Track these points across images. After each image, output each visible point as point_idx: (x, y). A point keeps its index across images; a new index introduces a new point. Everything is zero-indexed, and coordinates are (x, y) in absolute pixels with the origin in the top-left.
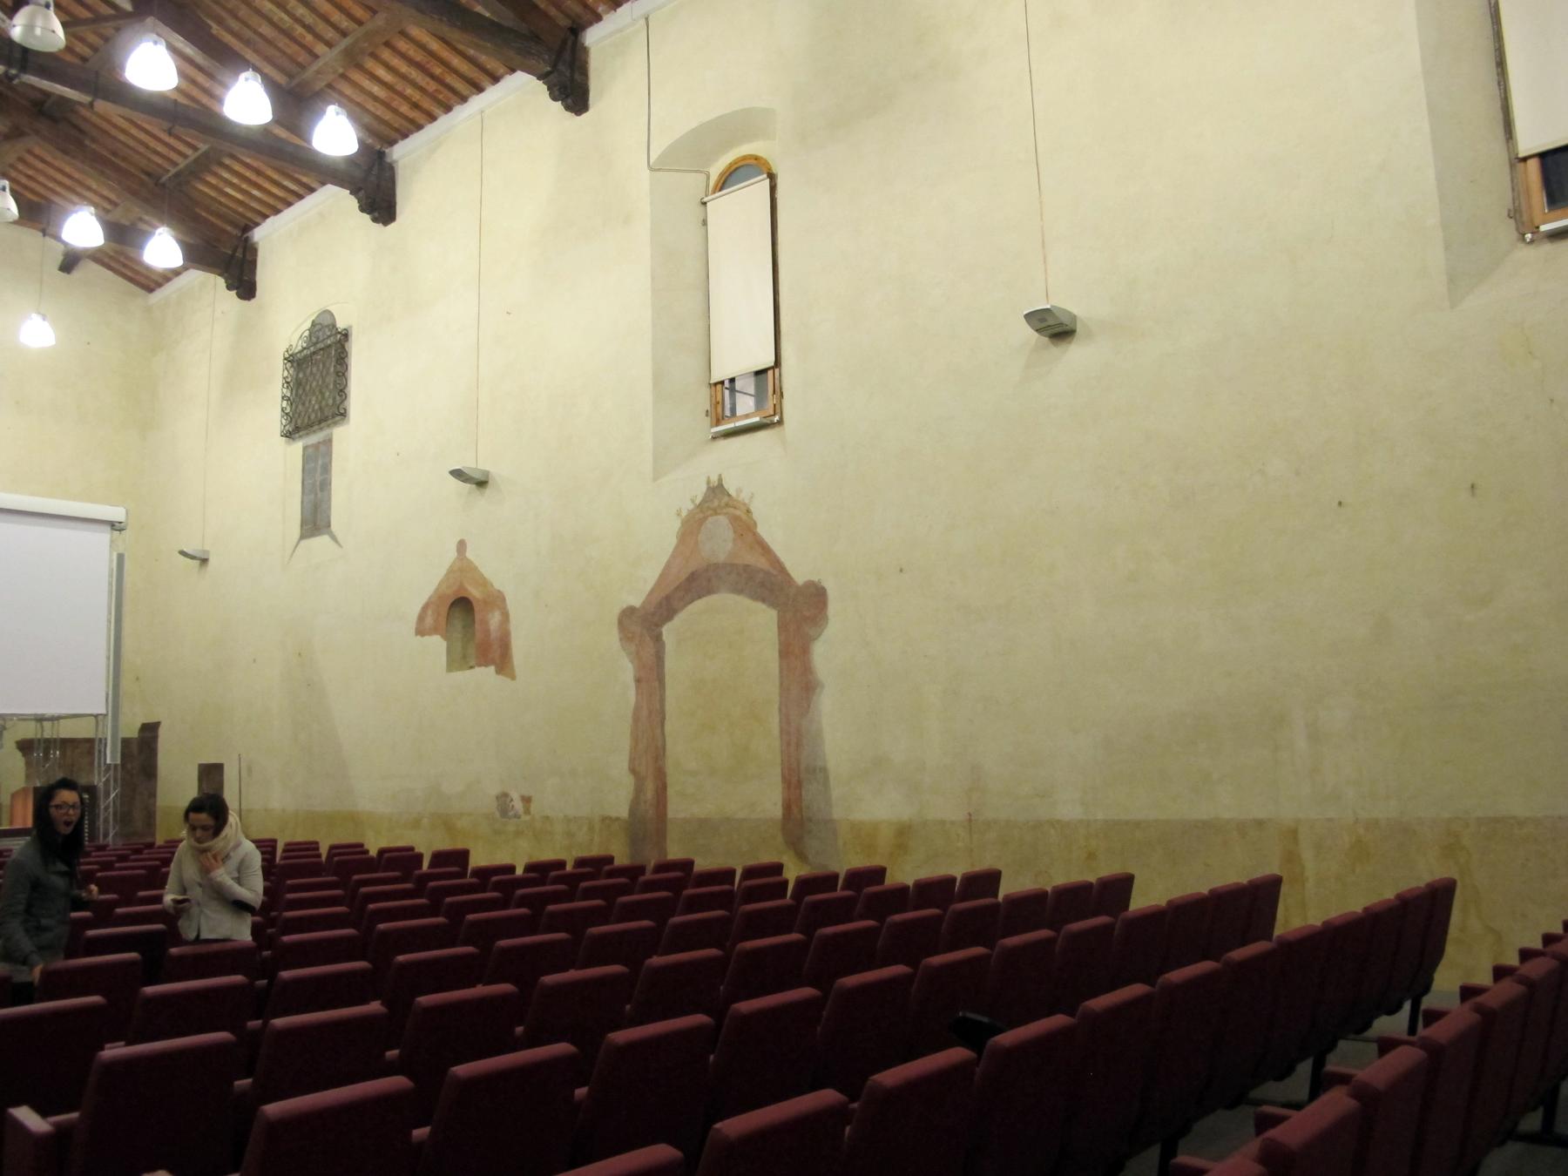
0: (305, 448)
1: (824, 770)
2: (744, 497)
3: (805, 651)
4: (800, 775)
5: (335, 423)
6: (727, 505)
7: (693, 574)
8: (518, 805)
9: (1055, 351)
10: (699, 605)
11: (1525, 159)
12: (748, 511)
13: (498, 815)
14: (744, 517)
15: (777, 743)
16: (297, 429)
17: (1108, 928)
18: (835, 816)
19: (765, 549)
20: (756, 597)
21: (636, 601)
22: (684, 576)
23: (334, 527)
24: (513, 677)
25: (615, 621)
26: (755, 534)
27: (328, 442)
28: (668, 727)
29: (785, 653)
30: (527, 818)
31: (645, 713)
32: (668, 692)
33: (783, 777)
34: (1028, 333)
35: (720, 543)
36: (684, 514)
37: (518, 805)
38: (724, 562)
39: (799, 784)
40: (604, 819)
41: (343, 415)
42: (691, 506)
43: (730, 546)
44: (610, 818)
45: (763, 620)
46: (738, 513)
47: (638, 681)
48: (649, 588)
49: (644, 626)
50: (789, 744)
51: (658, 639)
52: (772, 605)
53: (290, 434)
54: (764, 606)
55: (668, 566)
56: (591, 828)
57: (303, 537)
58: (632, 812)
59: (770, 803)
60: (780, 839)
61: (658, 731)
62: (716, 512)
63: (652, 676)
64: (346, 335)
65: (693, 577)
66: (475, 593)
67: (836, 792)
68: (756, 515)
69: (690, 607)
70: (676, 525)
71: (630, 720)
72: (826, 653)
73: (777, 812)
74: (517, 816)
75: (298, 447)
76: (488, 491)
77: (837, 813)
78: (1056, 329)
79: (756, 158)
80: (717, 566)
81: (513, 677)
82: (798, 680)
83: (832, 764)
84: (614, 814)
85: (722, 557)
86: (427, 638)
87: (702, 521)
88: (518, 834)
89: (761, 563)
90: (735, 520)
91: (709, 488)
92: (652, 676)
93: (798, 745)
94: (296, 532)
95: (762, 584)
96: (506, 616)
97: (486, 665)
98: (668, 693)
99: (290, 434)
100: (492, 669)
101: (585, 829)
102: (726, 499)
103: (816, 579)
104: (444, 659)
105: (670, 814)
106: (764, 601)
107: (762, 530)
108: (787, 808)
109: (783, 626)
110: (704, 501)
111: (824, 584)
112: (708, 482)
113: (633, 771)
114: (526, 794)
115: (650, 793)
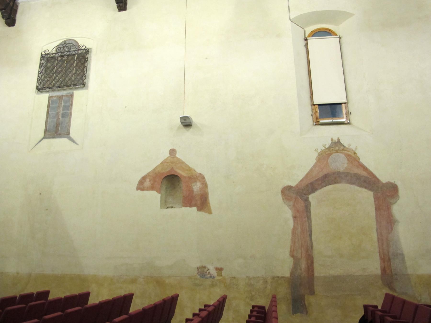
0: (50, 97)
1: (402, 255)
2: (353, 147)
3: (389, 208)
4: (389, 257)
5: (77, 89)
6: (343, 150)
7: (326, 175)
8: (213, 272)
9: (184, 130)
10: (330, 187)
11: (314, 105)
12: (355, 153)
13: (198, 277)
14: (353, 155)
15: (377, 245)
16: (44, 88)
17: (43, 304)
18: (409, 273)
19: (365, 169)
20: (361, 186)
21: (293, 184)
22: (321, 175)
23: (72, 134)
24: (210, 213)
25: (280, 191)
26: (359, 162)
27: (72, 96)
28: (313, 237)
29: (378, 208)
30: (220, 278)
31: (299, 230)
32: (313, 222)
33: (381, 258)
34: (179, 122)
35: (340, 163)
36: (319, 151)
37: (213, 272)
38: (338, 171)
39: (389, 260)
40: (273, 278)
41: (83, 85)
42: (323, 148)
43: (346, 165)
44: (278, 277)
45: (366, 196)
46: (349, 153)
47: (295, 217)
48: (300, 178)
49: (299, 195)
50: (382, 245)
51: (307, 200)
52: (371, 190)
53: (40, 89)
54: (366, 190)
55: (311, 170)
56: (265, 281)
57: (45, 138)
58: (292, 274)
59: (374, 267)
60: (380, 282)
61: (308, 238)
62: (337, 152)
63: (303, 214)
64: (87, 51)
65: (326, 176)
66: (180, 172)
67: (408, 263)
68: (358, 155)
69: (325, 188)
70: (316, 155)
71: (290, 234)
72: (397, 209)
73: (379, 272)
74: (212, 277)
75: (45, 97)
76: (191, 130)
77: (410, 271)
78: (187, 123)
79: (330, 30)
80: (339, 173)
81: (210, 213)
82: (386, 220)
83: (405, 252)
84: (280, 275)
85: (342, 170)
86: (145, 192)
87: (330, 155)
88: (213, 285)
89: (364, 173)
90: (348, 156)
91: (332, 142)
92: (303, 214)
93: (388, 245)
94: (42, 135)
95: (365, 181)
96: (205, 185)
97: (191, 206)
98: (313, 222)
99: (40, 89)
100: (195, 208)
101: (261, 282)
102: (342, 147)
103: (393, 181)
104: (159, 203)
105: (316, 274)
106: (366, 188)
107: (362, 161)
108: (384, 270)
109: (376, 198)
110: (330, 147)
111: (396, 183)
112: (332, 140)
113: (292, 256)
114: (219, 266)
115: (303, 264)
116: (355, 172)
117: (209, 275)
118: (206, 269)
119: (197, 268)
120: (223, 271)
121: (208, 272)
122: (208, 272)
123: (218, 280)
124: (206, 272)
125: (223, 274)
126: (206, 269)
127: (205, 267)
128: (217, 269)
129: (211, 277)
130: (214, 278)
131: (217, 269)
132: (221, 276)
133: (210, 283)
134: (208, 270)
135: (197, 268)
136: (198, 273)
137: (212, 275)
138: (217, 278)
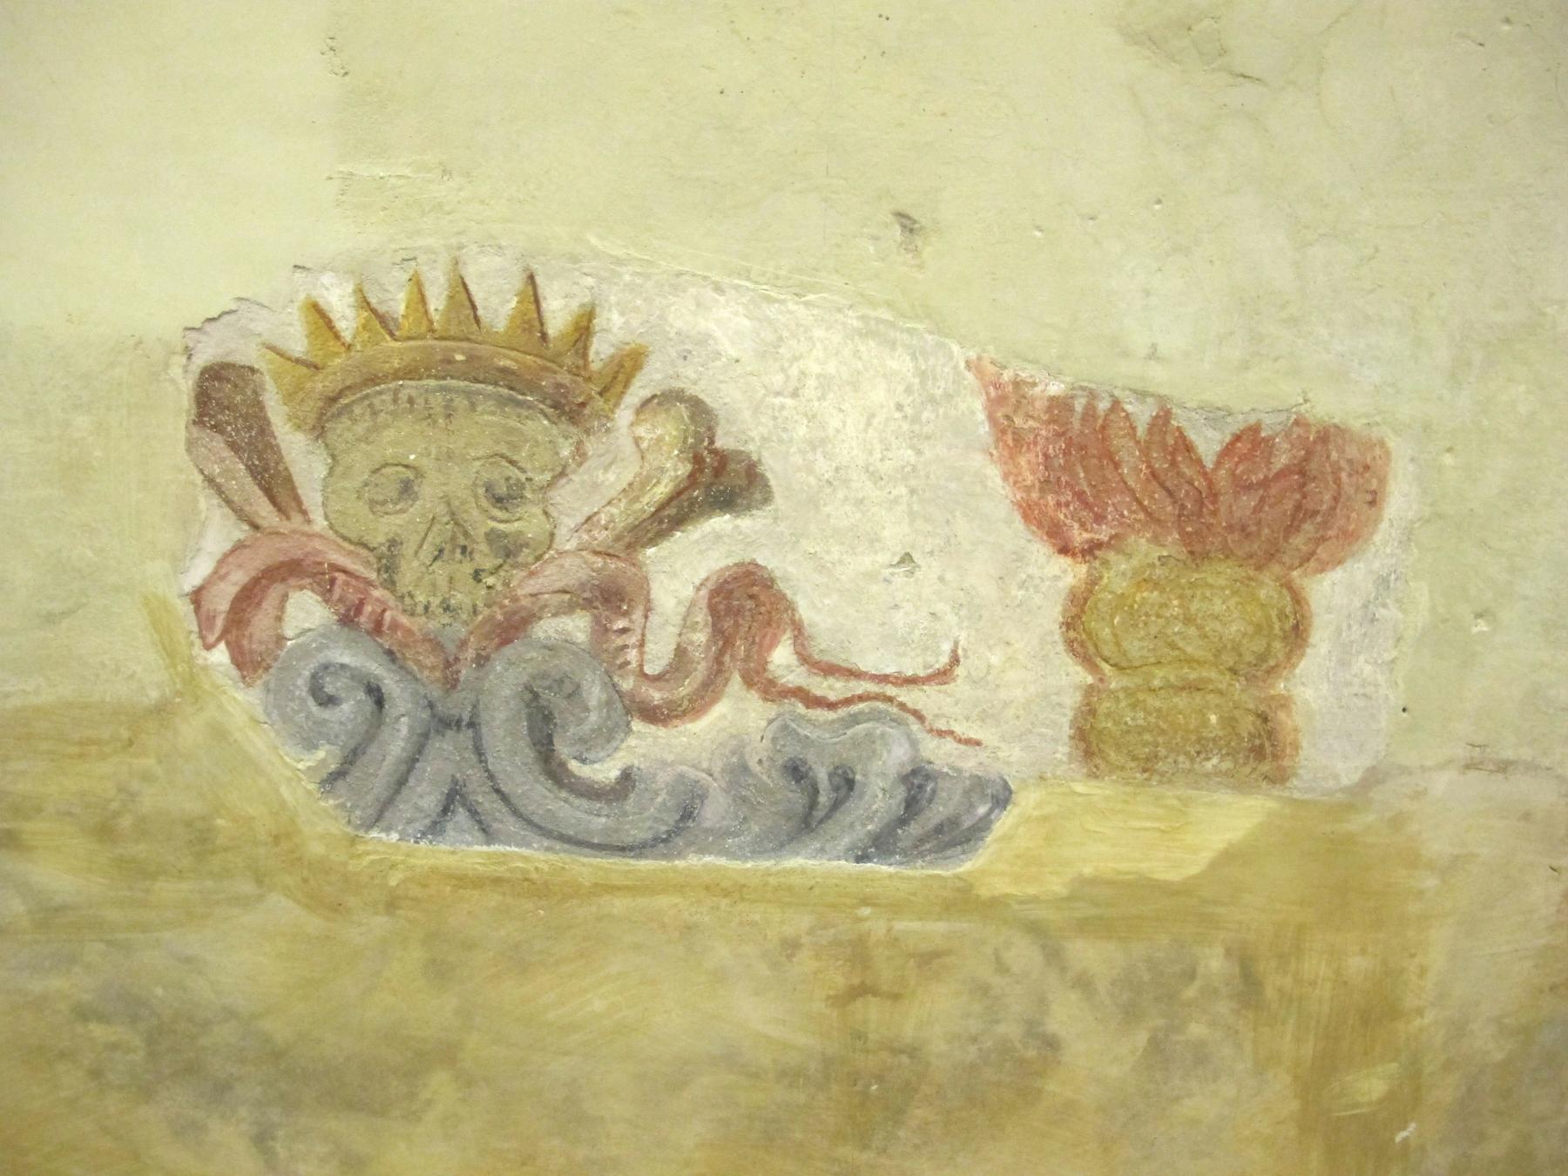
8: (923, 583)
13: (260, 753)
37: (923, 583)
61: (1080, 799)
108: (588, 604)
114: (1180, 343)
116: (1221, 846)
117: (738, 716)
118: (628, 459)
119: (222, 400)
120: (1332, 592)
121: (680, 571)
122: (680, 571)
123: (1113, 908)
124: (612, 598)
125: (1310, 686)
126: (628, 459)
127: (557, 377)
128: (1092, 469)
129: (809, 798)
130: (932, 817)
131: (1092, 469)
132: (1262, 749)
133: (766, 1016)
134: (720, 481)
135: (222, 400)
136: (238, 618)
137: (885, 696)
138: (1067, 835)
